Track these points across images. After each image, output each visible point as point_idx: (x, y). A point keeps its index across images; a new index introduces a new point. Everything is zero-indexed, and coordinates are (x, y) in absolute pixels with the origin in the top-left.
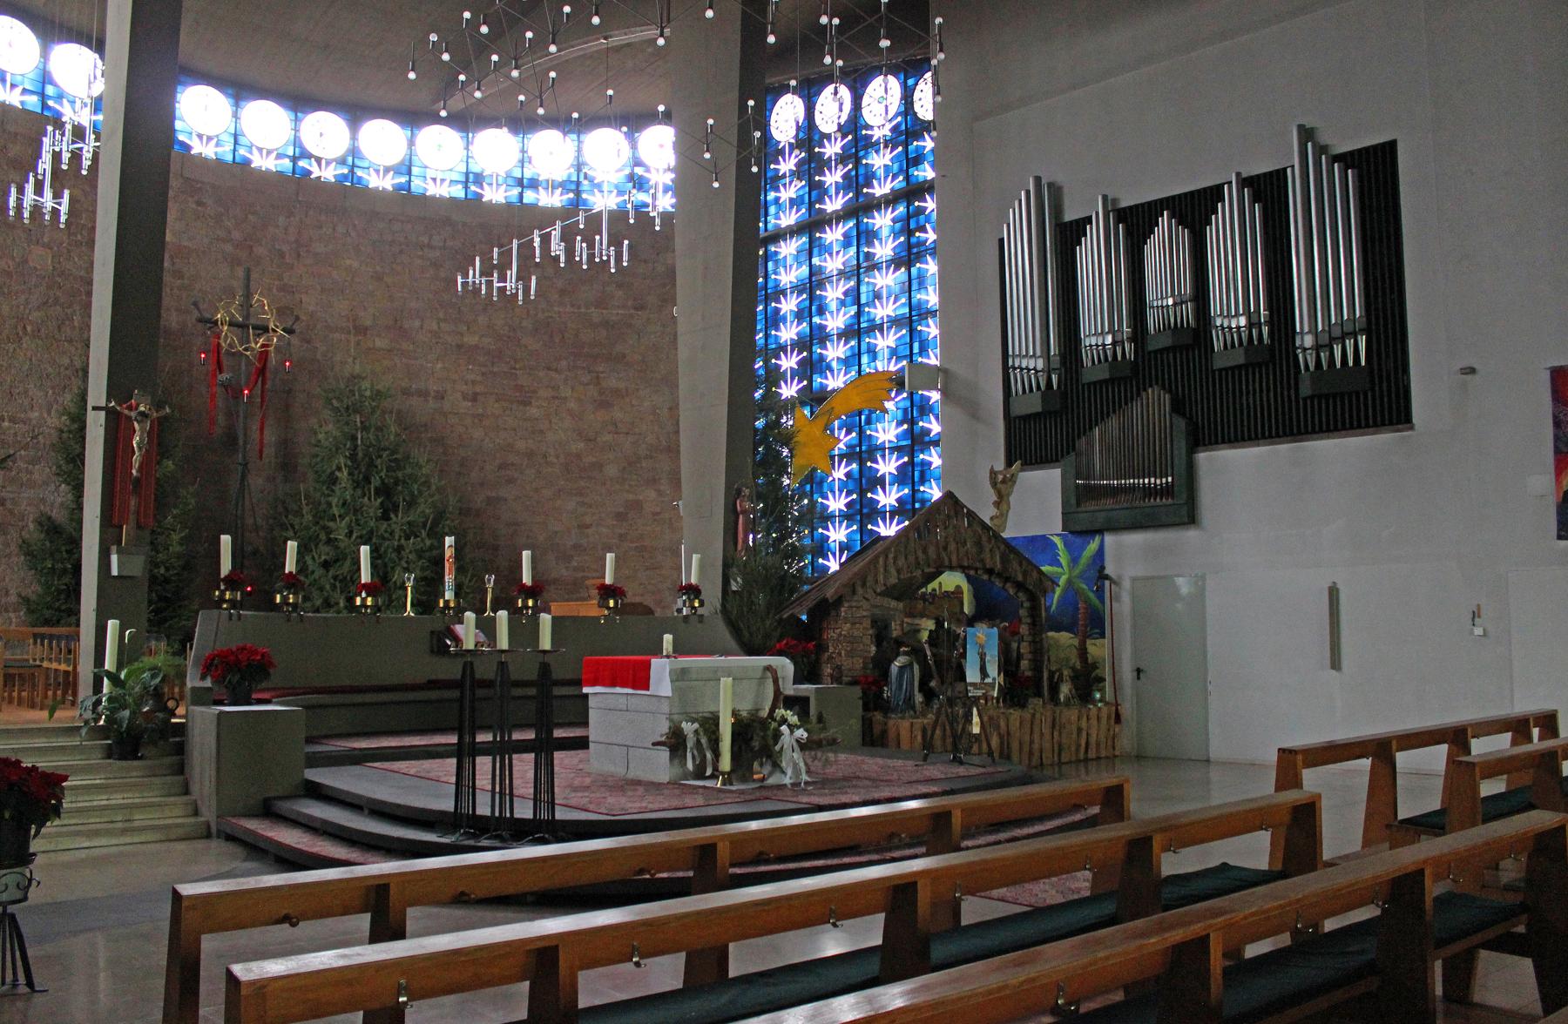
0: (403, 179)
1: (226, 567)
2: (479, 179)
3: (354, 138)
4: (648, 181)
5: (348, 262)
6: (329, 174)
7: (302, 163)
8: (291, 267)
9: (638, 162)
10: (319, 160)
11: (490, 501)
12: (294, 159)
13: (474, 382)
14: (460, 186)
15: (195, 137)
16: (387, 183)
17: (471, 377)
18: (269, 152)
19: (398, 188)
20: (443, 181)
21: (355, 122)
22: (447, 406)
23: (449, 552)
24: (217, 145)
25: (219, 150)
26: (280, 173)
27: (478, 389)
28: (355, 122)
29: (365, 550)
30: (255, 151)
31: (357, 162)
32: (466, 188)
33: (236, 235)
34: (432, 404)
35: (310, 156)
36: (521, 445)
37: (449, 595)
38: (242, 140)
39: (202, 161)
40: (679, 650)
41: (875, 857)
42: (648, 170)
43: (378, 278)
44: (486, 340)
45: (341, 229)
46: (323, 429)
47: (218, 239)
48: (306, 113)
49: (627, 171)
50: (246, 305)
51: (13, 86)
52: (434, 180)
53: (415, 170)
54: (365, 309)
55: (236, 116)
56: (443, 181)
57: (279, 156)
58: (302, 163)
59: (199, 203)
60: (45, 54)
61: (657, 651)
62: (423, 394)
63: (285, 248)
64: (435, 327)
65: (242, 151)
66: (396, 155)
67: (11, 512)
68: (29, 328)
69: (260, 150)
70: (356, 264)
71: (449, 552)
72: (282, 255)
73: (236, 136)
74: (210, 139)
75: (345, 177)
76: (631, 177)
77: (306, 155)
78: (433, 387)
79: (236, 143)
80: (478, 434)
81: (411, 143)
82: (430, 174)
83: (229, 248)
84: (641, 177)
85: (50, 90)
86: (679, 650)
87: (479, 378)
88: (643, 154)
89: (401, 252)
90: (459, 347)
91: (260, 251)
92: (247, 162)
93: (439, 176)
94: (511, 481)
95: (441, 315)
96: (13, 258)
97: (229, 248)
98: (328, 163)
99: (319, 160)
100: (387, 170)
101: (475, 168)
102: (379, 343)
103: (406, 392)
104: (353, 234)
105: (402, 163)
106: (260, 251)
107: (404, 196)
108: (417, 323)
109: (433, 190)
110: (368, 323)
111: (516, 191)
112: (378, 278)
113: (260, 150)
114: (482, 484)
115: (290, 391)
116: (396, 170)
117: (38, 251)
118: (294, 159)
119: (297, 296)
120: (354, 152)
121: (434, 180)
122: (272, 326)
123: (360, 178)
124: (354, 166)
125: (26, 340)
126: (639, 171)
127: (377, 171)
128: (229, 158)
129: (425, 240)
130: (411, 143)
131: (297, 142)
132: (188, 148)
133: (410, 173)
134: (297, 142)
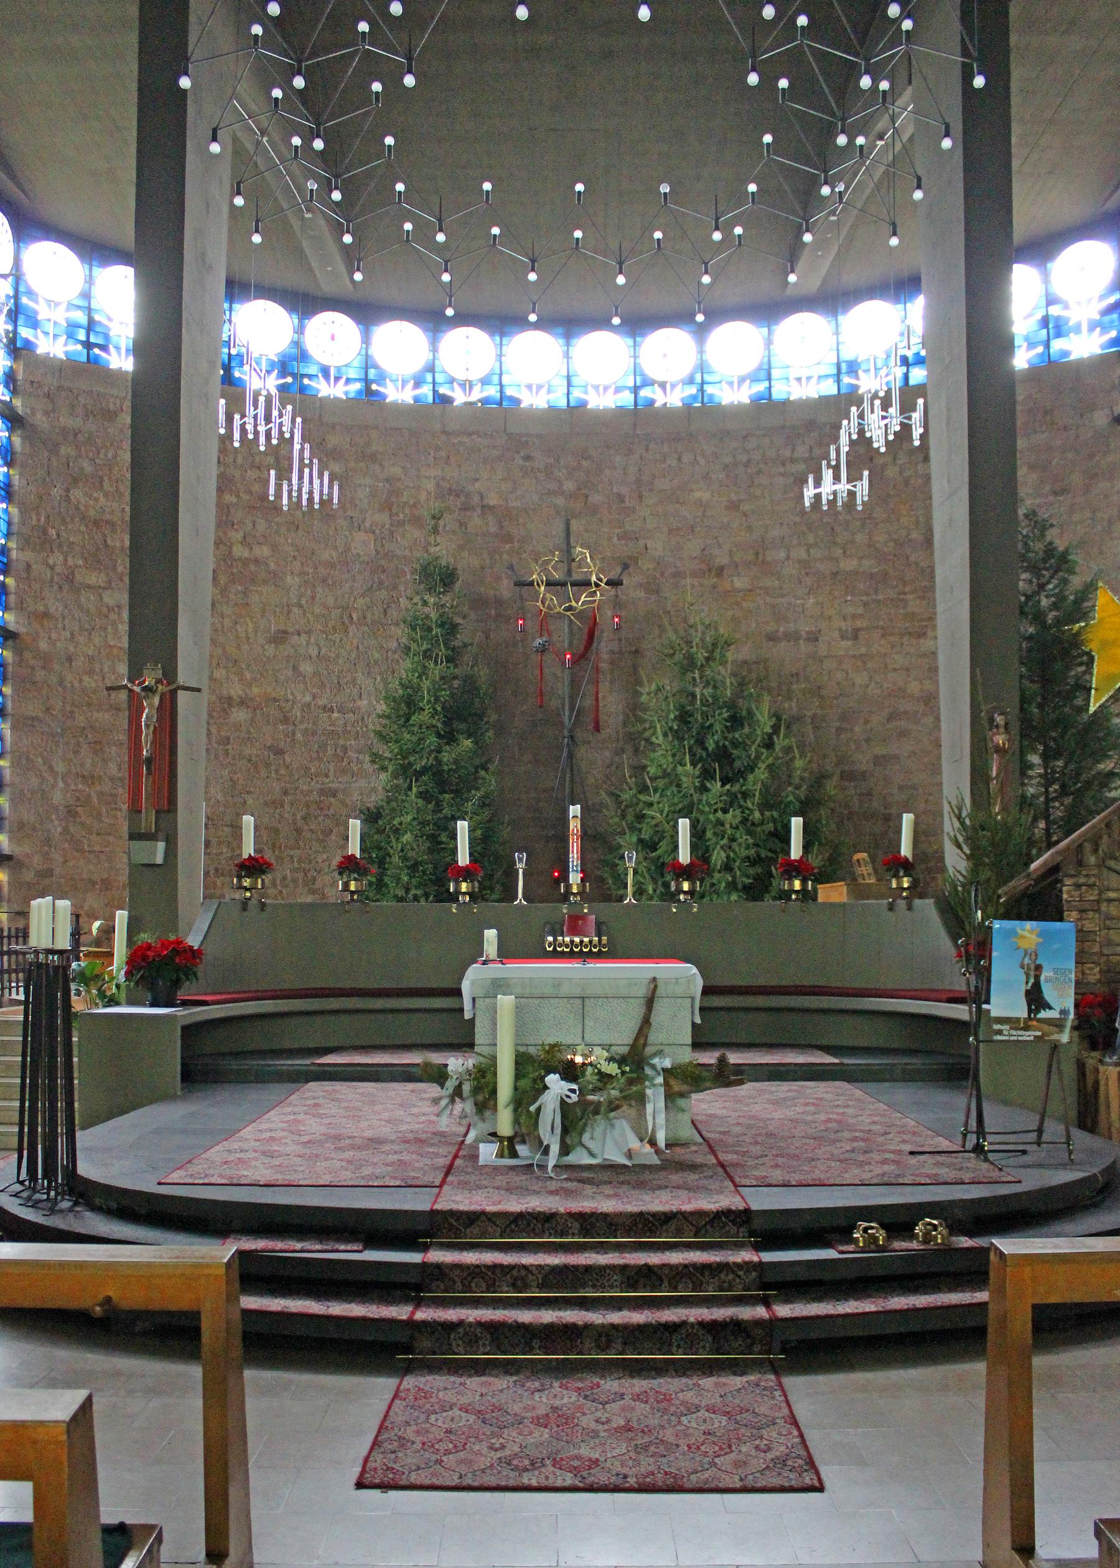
0: (761, 387)
1: (463, 858)
2: (853, 368)
3: (701, 352)
4: (1067, 320)
5: (698, 495)
6: (675, 399)
7: (645, 393)
8: (634, 510)
9: (1051, 301)
10: (663, 386)
11: (878, 761)
12: (636, 390)
13: (854, 617)
14: (831, 381)
15: (525, 391)
16: (742, 396)
17: (850, 610)
18: (606, 389)
19: (756, 400)
20: (809, 378)
21: (701, 332)
22: (823, 649)
23: (575, 826)
24: (549, 392)
25: (552, 397)
26: (620, 409)
27: (859, 624)
28: (701, 332)
29: (684, 824)
30: (590, 390)
31: (707, 378)
32: (838, 381)
33: (569, 486)
34: (804, 647)
35: (652, 383)
36: (914, 687)
37: (575, 878)
38: (575, 381)
39: (532, 415)
40: (506, 953)
41: (782, 1068)
42: (1066, 307)
43: (733, 506)
44: (867, 563)
45: (687, 458)
46: (659, 689)
47: (549, 493)
48: (644, 335)
49: (1040, 314)
50: (569, 558)
51: (337, 379)
52: (799, 380)
53: (775, 373)
54: (720, 546)
55: (567, 356)
56: (809, 378)
57: (618, 390)
58: (645, 393)
59: (528, 458)
60: (366, 340)
61: (475, 953)
62: (792, 637)
63: (624, 491)
64: (803, 555)
65: (576, 394)
66: (751, 362)
67: (343, 803)
68: (355, 616)
69: (596, 387)
70: (706, 496)
71: (575, 826)
72: (621, 498)
73: (569, 378)
74: (539, 387)
75: (694, 398)
76: (1045, 322)
77: (648, 382)
78: (804, 628)
79: (569, 385)
80: (860, 679)
81: (769, 342)
82: (793, 374)
83: (560, 501)
84: (1058, 319)
85: (372, 373)
86: (506, 953)
87: (860, 611)
88: (1058, 288)
89: (759, 472)
90: (835, 574)
91: (595, 498)
92: (583, 404)
93: (803, 375)
94: (903, 734)
95: (811, 540)
96: (336, 548)
97: (560, 501)
98: (673, 386)
99: (663, 386)
100: (742, 380)
101: (847, 355)
102: (739, 583)
103: (772, 638)
104: (702, 461)
105: (760, 368)
106: (595, 498)
107: (764, 406)
108: (783, 554)
109: (797, 393)
110: (725, 560)
111: (900, 371)
112: (733, 506)
113: (596, 387)
114: (868, 740)
115: (637, 652)
116: (754, 379)
117: (360, 536)
118: (636, 390)
119: (641, 542)
120: (702, 367)
121: (799, 380)
122: (594, 579)
123: (711, 396)
124: (703, 383)
125: (352, 629)
126: (1055, 311)
127: (731, 384)
128: (563, 404)
129: (787, 453)
130: (769, 342)
131: (636, 370)
132: (518, 401)
133: (769, 379)
134: (636, 370)
